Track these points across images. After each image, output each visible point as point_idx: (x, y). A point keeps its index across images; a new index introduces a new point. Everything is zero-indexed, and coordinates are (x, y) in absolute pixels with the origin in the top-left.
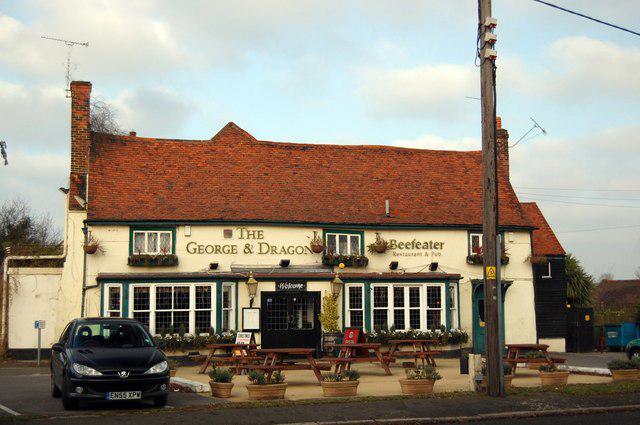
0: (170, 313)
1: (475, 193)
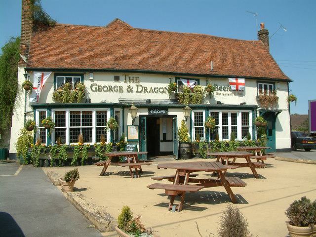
0: (79, 129)
1: (256, 61)
